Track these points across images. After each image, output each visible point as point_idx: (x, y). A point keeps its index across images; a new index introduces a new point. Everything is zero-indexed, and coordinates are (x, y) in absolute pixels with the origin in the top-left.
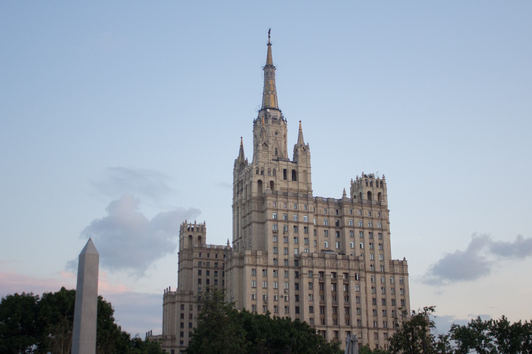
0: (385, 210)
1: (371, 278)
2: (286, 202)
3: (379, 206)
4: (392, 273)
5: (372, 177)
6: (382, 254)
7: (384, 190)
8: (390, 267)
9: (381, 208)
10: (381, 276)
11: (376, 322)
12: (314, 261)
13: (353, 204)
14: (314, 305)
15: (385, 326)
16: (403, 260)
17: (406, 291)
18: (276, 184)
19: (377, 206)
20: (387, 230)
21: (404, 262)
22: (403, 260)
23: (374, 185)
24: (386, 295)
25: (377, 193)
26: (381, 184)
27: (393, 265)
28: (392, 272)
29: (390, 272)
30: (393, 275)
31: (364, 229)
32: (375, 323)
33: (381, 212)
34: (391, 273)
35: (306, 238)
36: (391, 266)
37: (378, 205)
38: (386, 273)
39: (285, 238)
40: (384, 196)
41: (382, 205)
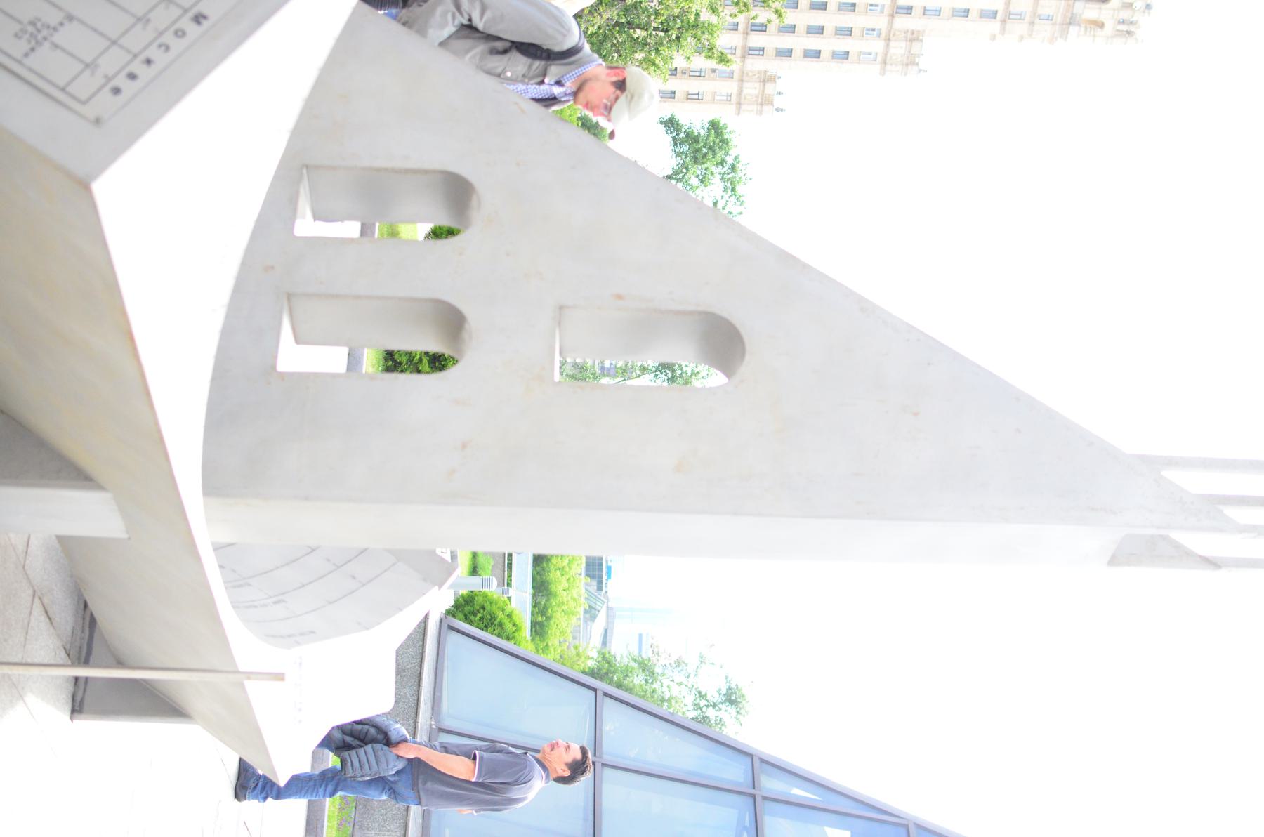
0: (1056, 35)
1: (874, 27)
2: (1054, 21)
3: (1068, 21)
4: (891, 35)
5: (1147, 11)
6: (942, 13)
7: (1116, 12)
8: (907, 32)
9: (1063, 24)
10: (886, 6)
11: (761, 53)
12: (903, 44)
13: (1066, 24)
14: (798, 36)
15: (751, 52)
16: (921, 66)
17: (840, 65)
18: (1100, 8)
19: (1070, 15)
20: (1003, 34)
21: (915, 68)
22: (921, 66)
23: (1125, 15)
24: (834, 14)
25: (1102, 19)
26: (1125, 33)
27: (912, 40)
28: (894, 35)
29: (892, 31)
30: (886, 36)
31: (1001, 21)
32: (760, 50)
33: (1053, 24)
34: (890, 31)
35: (968, 12)
36: (909, 36)
37: (1071, 18)
38: (892, 20)
39: (964, 12)
40: (1094, 36)
41: (1069, 28)
